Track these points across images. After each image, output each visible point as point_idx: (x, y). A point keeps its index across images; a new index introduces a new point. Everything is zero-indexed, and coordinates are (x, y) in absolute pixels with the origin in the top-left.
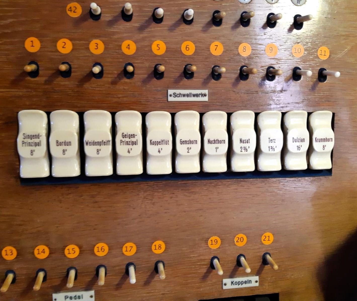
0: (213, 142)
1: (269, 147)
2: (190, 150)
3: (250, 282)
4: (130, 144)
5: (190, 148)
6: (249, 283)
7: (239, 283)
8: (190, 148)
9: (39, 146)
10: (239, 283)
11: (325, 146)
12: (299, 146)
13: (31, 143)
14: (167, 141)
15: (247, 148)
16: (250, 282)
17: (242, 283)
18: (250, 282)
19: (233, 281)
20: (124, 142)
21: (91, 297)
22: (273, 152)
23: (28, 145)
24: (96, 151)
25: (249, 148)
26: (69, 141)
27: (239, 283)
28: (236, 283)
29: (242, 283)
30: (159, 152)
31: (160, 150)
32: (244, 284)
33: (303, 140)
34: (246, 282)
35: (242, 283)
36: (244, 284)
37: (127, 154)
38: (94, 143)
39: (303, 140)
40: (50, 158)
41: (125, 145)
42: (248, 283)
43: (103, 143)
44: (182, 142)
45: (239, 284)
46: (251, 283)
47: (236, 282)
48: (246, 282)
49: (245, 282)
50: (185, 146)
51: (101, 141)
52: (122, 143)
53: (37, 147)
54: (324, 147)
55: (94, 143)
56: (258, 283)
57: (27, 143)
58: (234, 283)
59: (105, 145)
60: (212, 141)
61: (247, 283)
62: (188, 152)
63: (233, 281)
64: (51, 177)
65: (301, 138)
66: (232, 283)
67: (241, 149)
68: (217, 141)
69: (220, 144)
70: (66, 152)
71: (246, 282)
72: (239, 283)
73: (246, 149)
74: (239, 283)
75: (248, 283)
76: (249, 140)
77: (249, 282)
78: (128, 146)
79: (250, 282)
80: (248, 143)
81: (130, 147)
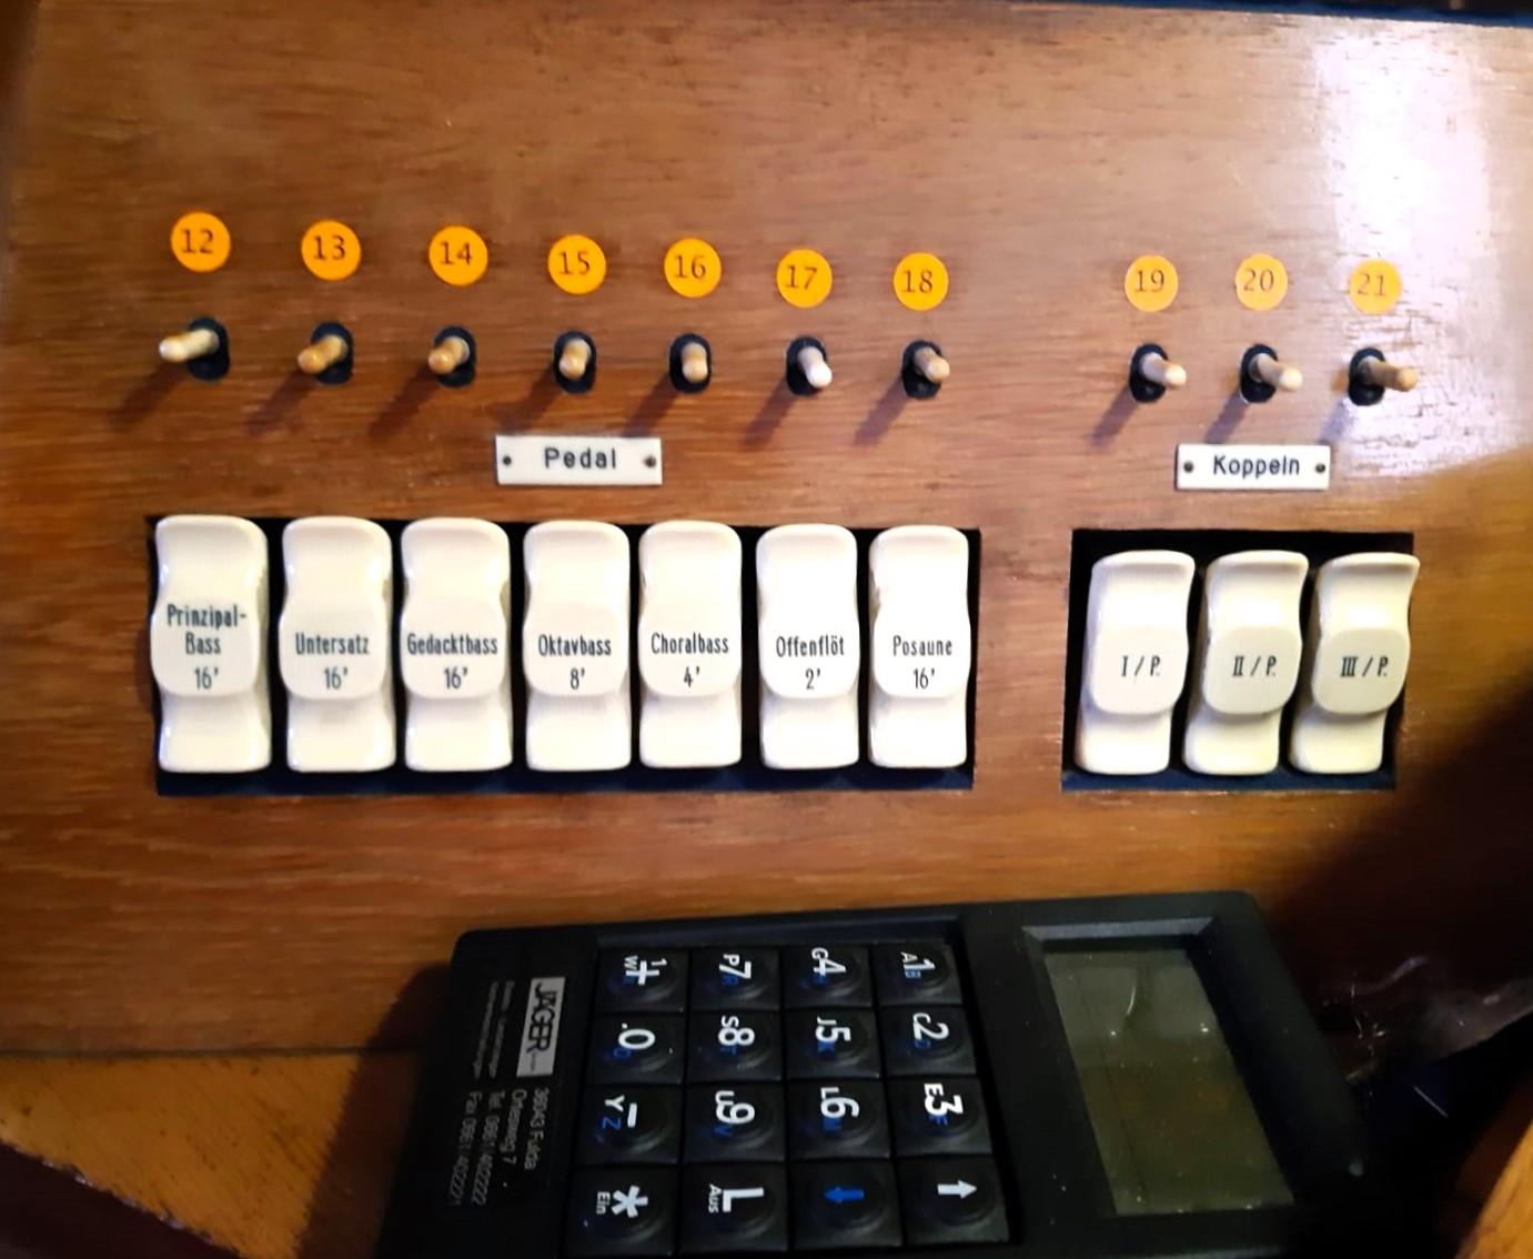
3: (1294, 466)
5: (815, 673)
11: (815, 673)
12: (924, 670)
13: (201, 616)
14: (838, 641)
18: (1294, 466)
19: (1223, 458)
30: (688, 679)
31: (693, 672)
34: (1274, 467)
35: (1257, 468)
36: (1268, 471)
50: (563, 664)
52: (174, 619)
54: (575, 675)
58: (1225, 464)
60: (442, 641)
63: (1223, 458)
64: (752, 771)
68: (465, 643)
71: (1274, 467)
74: (1246, 468)
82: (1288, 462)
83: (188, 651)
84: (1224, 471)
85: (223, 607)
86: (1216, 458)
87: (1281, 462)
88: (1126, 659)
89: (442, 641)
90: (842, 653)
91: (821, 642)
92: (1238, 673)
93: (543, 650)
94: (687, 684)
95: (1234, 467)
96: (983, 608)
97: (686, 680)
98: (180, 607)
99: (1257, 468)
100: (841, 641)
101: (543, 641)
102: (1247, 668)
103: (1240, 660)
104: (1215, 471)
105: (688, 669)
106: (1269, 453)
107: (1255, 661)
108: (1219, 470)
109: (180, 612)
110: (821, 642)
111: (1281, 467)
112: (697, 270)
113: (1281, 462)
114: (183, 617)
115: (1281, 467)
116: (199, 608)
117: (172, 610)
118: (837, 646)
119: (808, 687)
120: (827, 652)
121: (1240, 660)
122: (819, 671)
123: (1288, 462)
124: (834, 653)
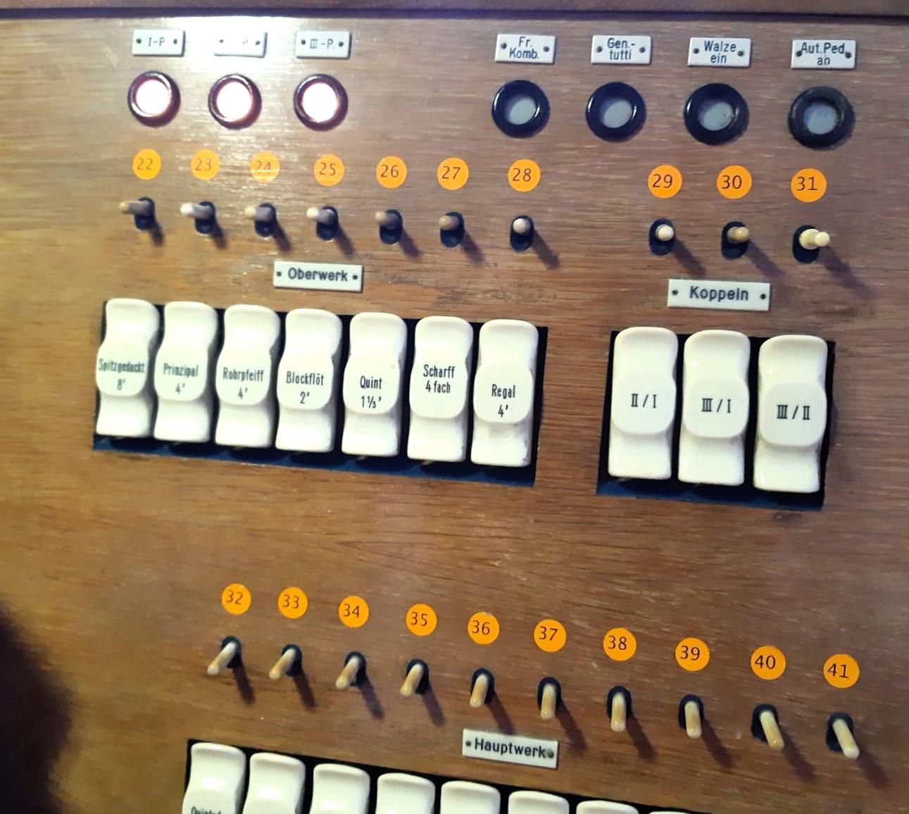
0: (445, 388)
1: (363, 398)
2: (306, 397)
3: (745, 295)
4: (183, 372)
5: (306, 394)
6: (740, 299)
7: (722, 293)
8: (308, 393)
9: (193, 375)
10: (722, 293)
13: (180, 370)
14: (320, 376)
15: (376, 399)
16: (744, 295)
17: (711, 295)
18: (745, 295)
19: (697, 288)
20: (171, 370)
21: (763, 297)
22: (372, 411)
23: (175, 372)
24: (117, 383)
25: (507, 408)
26: (776, 409)
27: (720, 295)
28: (704, 294)
29: (722, 296)
31: (243, 391)
32: (726, 297)
33: (191, 372)
34: (731, 295)
35: (721, 295)
36: (726, 297)
37: (498, 418)
38: (234, 375)
39: (191, 372)
40: (469, 417)
41: (173, 373)
42: (738, 299)
43: (249, 374)
44: (291, 378)
45: (713, 295)
46: (747, 299)
47: (704, 290)
48: (731, 293)
49: (729, 295)
51: (245, 371)
52: (167, 371)
53: (190, 377)
54: (120, 382)
55: (234, 375)
56: (671, 289)
57: (173, 368)
58: (698, 291)
59: (251, 380)
60: (441, 385)
61: (735, 298)
62: (302, 402)
63: (697, 288)
65: (374, 379)
66: (693, 291)
67: (302, 398)
69: (228, 379)
70: (124, 385)
71: (731, 295)
72: (720, 295)
73: (372, 403)
74: (712, 295)
75: (738, 299)
76: (380, 381)
77: (740, 295)
78: (179, 377)
79: (744, 295)
80: (512, 398)
81: (182, 379)
82: (740, 292)
83: (287, 382)
84: (697, 297)
85: (192, 366)
86: (692, 287)
87: (736, 292)
88: (729, 412)
89: (441, 385)
90: (322, 384)
91: (311, 377)
92: (634, 405)
93: (363, 384)
94: (240, 397)
95: (704, 294)
96: (186, 757)
97: (427, 388)
98: (170, 365)
99: (721, 295)
100: (322, 377)
101: (363, 379)
102: (640, 402)
103: (635, 396)
104: (691, 297)
105: (241, 389)
106: (727, 286)
107: (795, 408)
108: (694, 296)
109: (170, 368)
110: (311, 377)
111: (736, 295)
112: (484, 628)
113: (736, 292)
114: (171, 370)
115: (736, 295)
116: (180, 366)
117: (166, 367)
118: (319, 380)
119: (302, 402)
120: (314, 383)
121: (635, 396)
122: (308, 393)
123: (740, 292)
124: (318, 384)
